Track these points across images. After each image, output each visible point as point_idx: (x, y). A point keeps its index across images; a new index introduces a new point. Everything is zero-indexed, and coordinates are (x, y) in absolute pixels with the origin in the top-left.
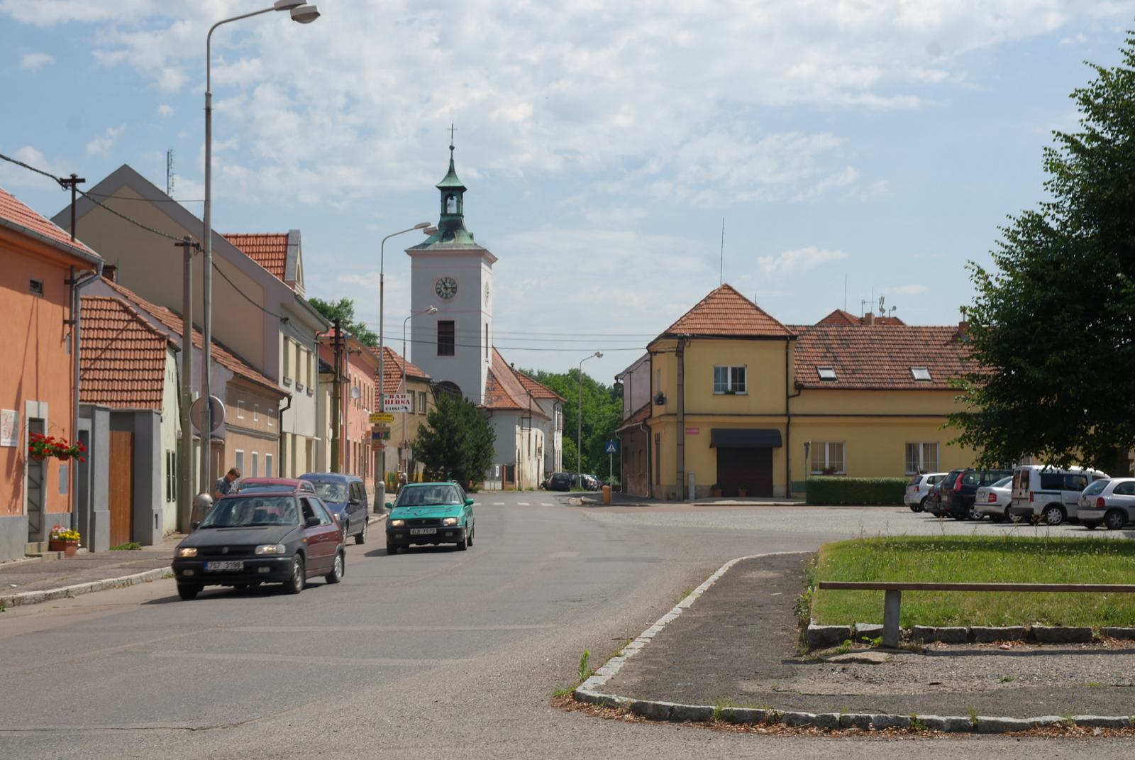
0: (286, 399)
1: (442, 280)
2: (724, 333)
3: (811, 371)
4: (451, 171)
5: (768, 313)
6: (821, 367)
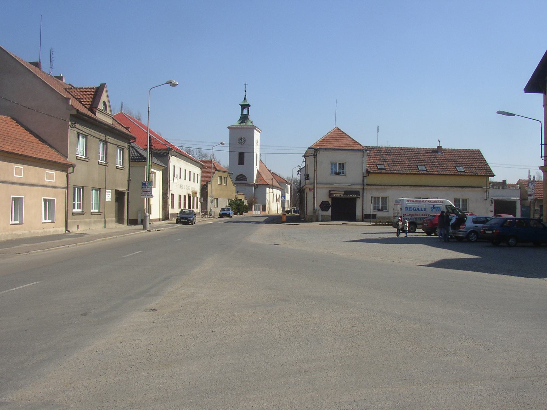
0: (72, 168)
1: (242, 137)
2: (335, 148)
3: (374, 166)
4: (245, 99)
5: (355, 140)
6: (378, 164)
